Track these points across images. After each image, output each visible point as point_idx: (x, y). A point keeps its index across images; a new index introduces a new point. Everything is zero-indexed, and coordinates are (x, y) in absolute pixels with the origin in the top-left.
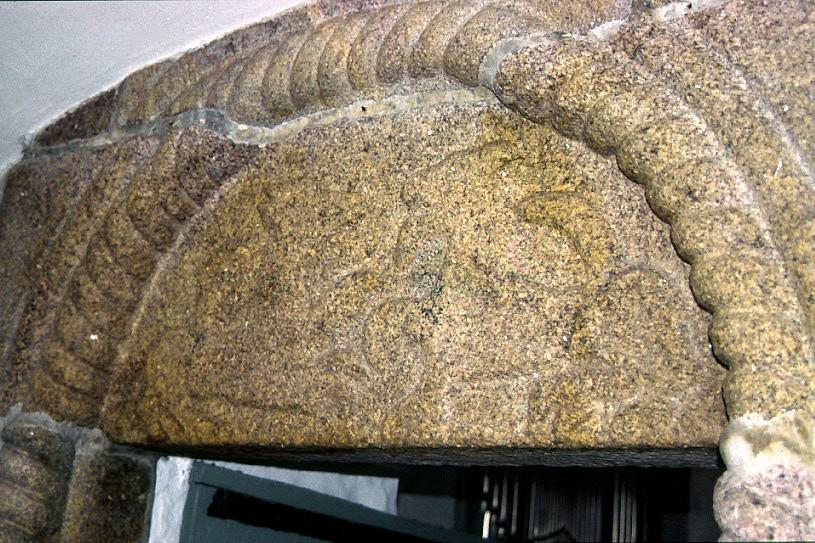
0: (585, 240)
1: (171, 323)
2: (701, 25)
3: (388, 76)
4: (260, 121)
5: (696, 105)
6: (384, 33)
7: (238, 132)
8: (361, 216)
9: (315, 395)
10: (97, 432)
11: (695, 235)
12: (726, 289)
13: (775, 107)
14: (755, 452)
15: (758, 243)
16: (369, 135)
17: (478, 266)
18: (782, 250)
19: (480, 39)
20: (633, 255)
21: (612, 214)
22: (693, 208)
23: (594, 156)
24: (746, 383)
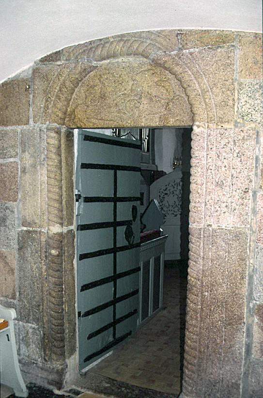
0: (169, 90)
1: (79, 103)
2: (191, 55)
3: (129, 55)
4: (99, 61)
5: (190, 70)
6: (128, 46)
7: (94, 63)
8: (123, 82)
9: (116, 118)
10: (65, 126)
11: (189, 93)
12: (194, 103)
13: (203, 72)
14: (198, 128)
15: (199, 95)
16: (124, 65)
17: (149, 94)
18: (203, 96)
19: (149, 51)
20: (178, 93)
21: (174, 85)
22: (189, 88)
23: (170, 74)
24: (197, 117)
